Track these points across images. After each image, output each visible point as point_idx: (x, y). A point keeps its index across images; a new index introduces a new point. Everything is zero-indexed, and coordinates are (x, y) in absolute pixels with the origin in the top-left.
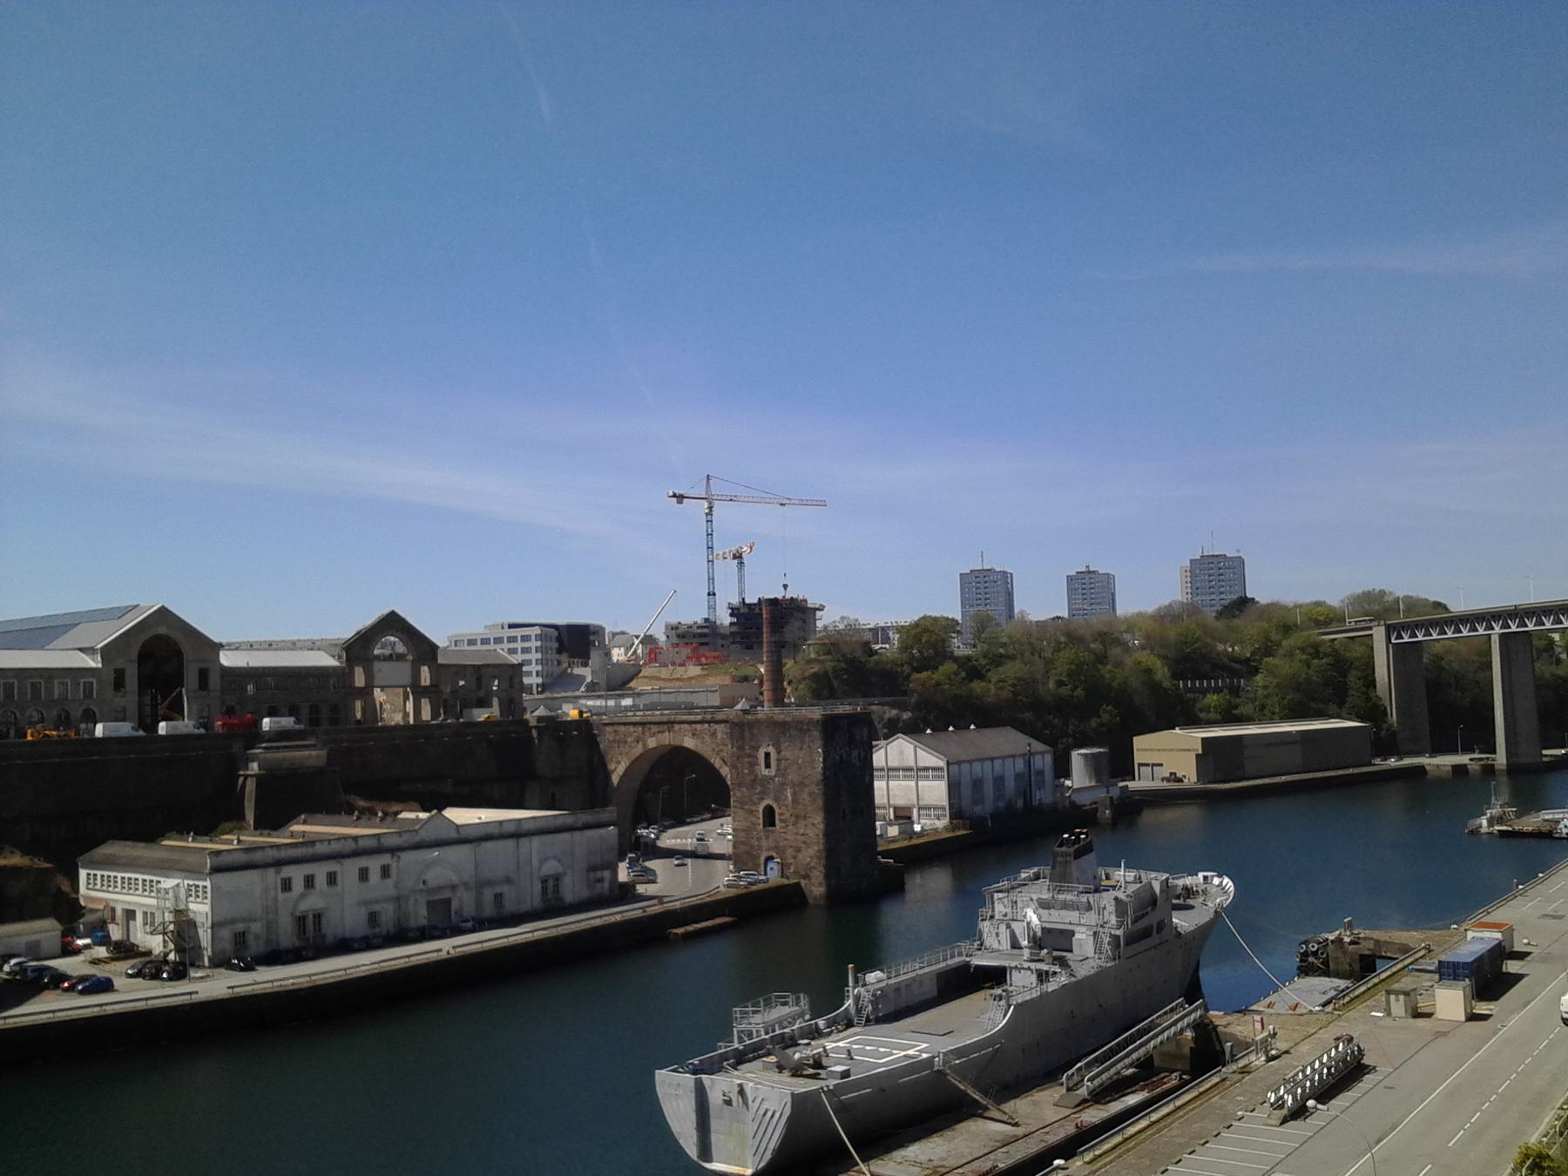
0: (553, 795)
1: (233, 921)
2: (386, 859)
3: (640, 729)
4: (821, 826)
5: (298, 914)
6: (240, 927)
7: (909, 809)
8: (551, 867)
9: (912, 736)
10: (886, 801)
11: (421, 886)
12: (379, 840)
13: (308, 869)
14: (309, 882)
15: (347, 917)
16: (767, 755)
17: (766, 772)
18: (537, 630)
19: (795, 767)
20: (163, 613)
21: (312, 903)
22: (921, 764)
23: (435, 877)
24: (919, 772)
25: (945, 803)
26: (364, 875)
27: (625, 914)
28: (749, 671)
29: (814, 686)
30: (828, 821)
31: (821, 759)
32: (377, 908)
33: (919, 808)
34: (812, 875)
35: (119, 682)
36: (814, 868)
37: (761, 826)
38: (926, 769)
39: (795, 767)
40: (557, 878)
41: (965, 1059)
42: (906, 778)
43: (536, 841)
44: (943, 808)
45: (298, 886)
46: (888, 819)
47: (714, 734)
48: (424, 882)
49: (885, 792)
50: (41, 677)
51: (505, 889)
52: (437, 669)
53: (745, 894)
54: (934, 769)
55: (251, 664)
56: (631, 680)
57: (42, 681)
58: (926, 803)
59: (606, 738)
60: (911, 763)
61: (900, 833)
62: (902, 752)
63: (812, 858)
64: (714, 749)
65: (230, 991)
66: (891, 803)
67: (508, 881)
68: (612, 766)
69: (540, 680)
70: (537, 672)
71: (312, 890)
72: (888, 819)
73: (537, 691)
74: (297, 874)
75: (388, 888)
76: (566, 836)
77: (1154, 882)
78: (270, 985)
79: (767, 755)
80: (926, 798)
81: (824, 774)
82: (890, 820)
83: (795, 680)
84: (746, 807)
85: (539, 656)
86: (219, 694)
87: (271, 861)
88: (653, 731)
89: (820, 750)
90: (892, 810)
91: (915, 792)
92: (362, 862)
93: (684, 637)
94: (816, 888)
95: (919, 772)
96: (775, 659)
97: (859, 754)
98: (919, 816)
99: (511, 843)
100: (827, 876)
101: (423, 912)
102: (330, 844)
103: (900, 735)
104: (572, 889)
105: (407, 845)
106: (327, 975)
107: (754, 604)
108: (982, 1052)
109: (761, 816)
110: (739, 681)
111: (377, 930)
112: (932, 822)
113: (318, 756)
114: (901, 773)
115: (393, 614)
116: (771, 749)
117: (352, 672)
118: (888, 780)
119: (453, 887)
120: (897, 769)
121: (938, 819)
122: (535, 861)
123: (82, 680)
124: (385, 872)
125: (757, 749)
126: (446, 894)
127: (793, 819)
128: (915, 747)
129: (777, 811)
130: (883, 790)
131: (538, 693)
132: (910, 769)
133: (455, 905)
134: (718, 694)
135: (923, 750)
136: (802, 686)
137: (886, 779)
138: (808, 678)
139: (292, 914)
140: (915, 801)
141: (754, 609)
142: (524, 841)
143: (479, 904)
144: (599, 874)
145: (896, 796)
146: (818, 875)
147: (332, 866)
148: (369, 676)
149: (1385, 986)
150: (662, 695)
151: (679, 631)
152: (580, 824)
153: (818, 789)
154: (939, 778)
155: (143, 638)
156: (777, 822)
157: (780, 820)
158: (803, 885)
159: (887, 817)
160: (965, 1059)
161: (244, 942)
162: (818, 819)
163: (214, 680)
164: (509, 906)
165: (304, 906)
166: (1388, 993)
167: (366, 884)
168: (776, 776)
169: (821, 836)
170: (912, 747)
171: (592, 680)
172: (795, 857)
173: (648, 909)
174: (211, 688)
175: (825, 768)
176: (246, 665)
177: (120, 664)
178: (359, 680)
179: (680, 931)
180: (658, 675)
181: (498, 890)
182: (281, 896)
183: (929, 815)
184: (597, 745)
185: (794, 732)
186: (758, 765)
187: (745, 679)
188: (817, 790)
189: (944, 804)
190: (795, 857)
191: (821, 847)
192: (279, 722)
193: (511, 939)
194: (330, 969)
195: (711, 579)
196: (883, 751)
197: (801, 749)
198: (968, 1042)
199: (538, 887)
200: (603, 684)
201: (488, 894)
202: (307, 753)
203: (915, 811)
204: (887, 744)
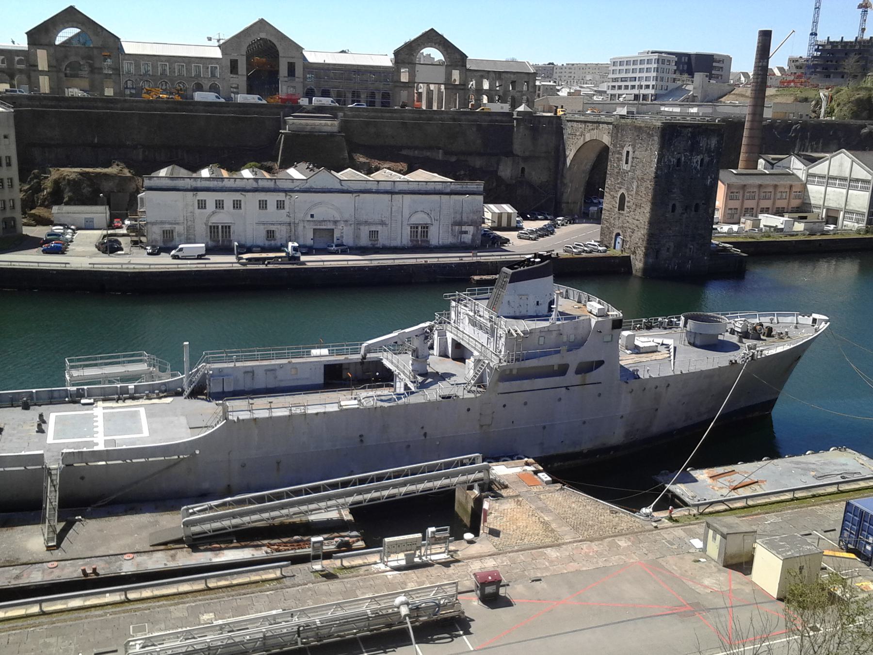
0: (523, 169)
1: (162, 223)
2: (281, 196)
3: (584, 125)
4: (648, 215)
5: (210, 224)
6: (167, 227)
7: (837, 211)
8: (420, 218)
9: (852, 152)
10: (821, 203)
11: (309, 218)
12: (275, 182)
13: (219, 196)
14: (219, 205)
15: (345, 234)
16: (628, 152)
17: (625, 167)
18: (656, 56)
19: (641, 165)
20: (262, 24)
21: (222, 218)
22: (854, 176)
23: (320, 213)
24: (850, 182)
25: (865, 210)
26: (263, 205)
27: (440, 259)
28: (810, 94)
29: (855, 108)
30: (653, 210)
31: (656, 160)
32: (272, 228)
33: (845, 212)
34: (637, 252)
35: (234, 67)
36: (639, 247)
37: (617, 210)
38: (857, 180)
39: (641, 165)
40: (426, 227)
41: (143, 460)
42: (841, 186)
43: (407, 197)
44: (863, 214)
45: (211, 206)
46: (820, 218)
48: (312, 216)
49: (823, 196)
50: (217, 63)
51: (379, 228)
52: (467, 73)
53: (571, 258)
54: (863, 181)
55: (327, 62)
56: (722, 97)
57: (218, 66)
58: (851, 208)
59: (568, 130)
60: (847, 175)
61: (804, 229)
62: (841, 165)
63: (639, 239)
65: (91, 266)
66: (826, 204)
67: (383, 223)
68: (567, 153)
69: (653, 92)
70: (653, 86)
71: (221, 211)
72: (820, 218)
73: (651, 99)
74: (210, 198)
75: (282, 215)
76: (437, 197)
77: (592, 320)
78: (120, 266)
79: (628, 152)
80: (852, 204)
81: (656, 173)
82: (822, 218)
83: (842, 103)
84: (612, 193)
85: (655, 74)
86: (302, 80)
87: (189, 187)
89: (656, 153)
90: (825, 210)
91: (844, 199)
92: (262, 196)
93: (801, 68)
94: (638, 264)
95: (850, 182)
96: (759, 80)
97: (702, 160)
98: (844, 218)
99: (387, 197)
100: (646, 255)
101: (310, 235)
102: (235, 181)
103: (844, 150)
104: (435, 237)
105: (297, 188)
106: (104, 266)
107: (837, 42)
108: (150, 459)
109: (618, 202)
110: (800, 101)
111: (273, 242)
112: (853, 224)
113: (332, 125)
114: (837, 182)
115: (262, 19)
116: (630, 149)
117: (399, 72)
118: (848, 189)
119: (335, 222)
120: (835, 178)
121: (858, 223)
122: (406, 213)
123: (210, 66)
124: (280, 205)
125: (623, 147)
126: (330, 226)
127: (634, 206)
128: (853, 161)
129: (627, 199)
130: (821, 194)
131: (652, 100)
132: (845, 179)
133: (337, 234)
134: (771, 109)
135: (858, 164)
136: (845, 108)
137: (825, 185)
138: (852, 102)
139: (206, 225)
140: (843, 206)
141: (837, 46)
142: (395, 196)
143: (357, 237)
144: (464, 228)
145: (830, 199)
146: (640, 253)
147: (237, 196)
148: (412, 74)
149: (709, 519)
150: (640, 106)
151: (798, 64)
152: (448, 190)
153: (651, 185)
154: (863, 189)
155: (249, 41)
156: (625, 207)
157: (627, 206)
158: (631, 258)
159: (820, 216)
160: (143, 460)
161: (273, 237)
162: (647, 208)
163: (299, 71)
164: (382, 241)
165: (215, 220)
166: (708, 526)
167: (264, 211)
168: (629, 171)
169: (647, 223)
170: (850, 160)
171: (693, 94)
172: (631, 237)
173: (464, 259)
174: (296, 75)
175: (657, 168)
176: (323, 62)
177: (234, 56)
178: (404, 78)
179: (476, 278)
180: (744, 93)
181: (373, 228)
182: (197, 211)
183: (851, 218)
184: (562, 135)
185: (644, 136)
186: (621, 161)
187: (806, 100)
188: (649, 185)
189: (865, 211)
190: (631, 237)
191: (646, 231)
192: (320, 101)
193: (350, 263)
194: (111, 262)
195: (815, 23)
196: (828, 162)
197: (646, 150)
198: (23, 453)
199: (407, 230)
200: (700, 96)
201: (365, 231)
202: (323, 122)
203: (842, 213)
204: (831, 157)
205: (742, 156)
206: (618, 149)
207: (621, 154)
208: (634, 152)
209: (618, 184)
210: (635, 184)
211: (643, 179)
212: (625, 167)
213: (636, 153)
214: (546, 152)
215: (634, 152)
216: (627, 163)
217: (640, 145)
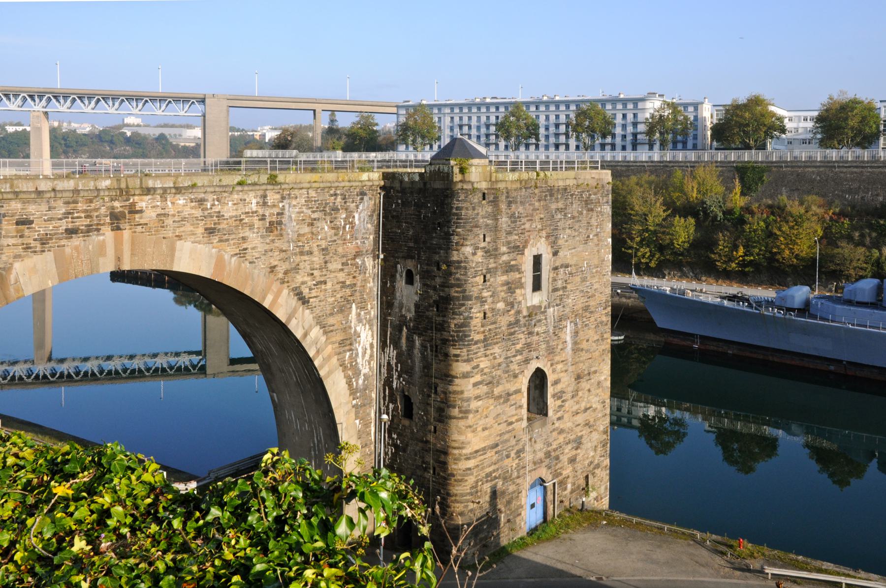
16: (537, 260)
47: (274, 227)
53: (732, 309)
64: (273, 269)
79: (537, 260)
88: (40, 228)
116: (541, 247)
125: (518, 250)
129: (551, 378)
179: (417, 343)
205: (616, 338)
206: (505, 258)
207: (519, 270)
208: (555, 254)
209: (519, 352)
210: (569, 328)
211: (586, 309)
212: (536, 299)
213: (561, 254)
214: (127, 187)
215: (555, 254)
216: (537, 287)
217: (568, 231)
